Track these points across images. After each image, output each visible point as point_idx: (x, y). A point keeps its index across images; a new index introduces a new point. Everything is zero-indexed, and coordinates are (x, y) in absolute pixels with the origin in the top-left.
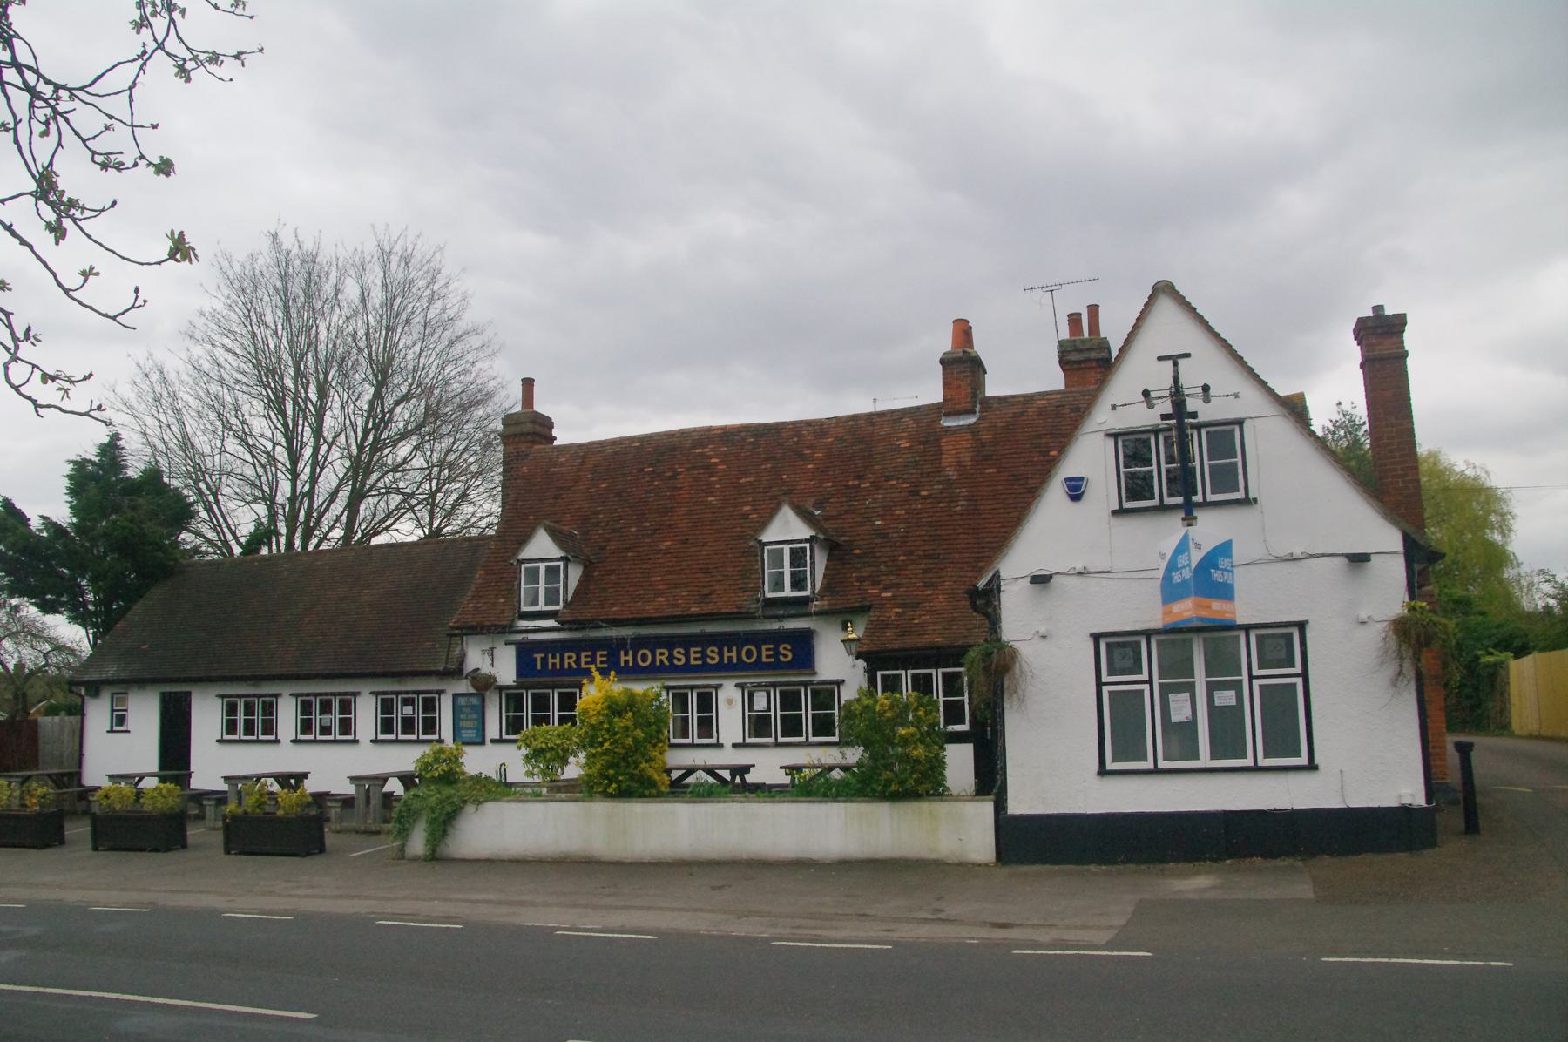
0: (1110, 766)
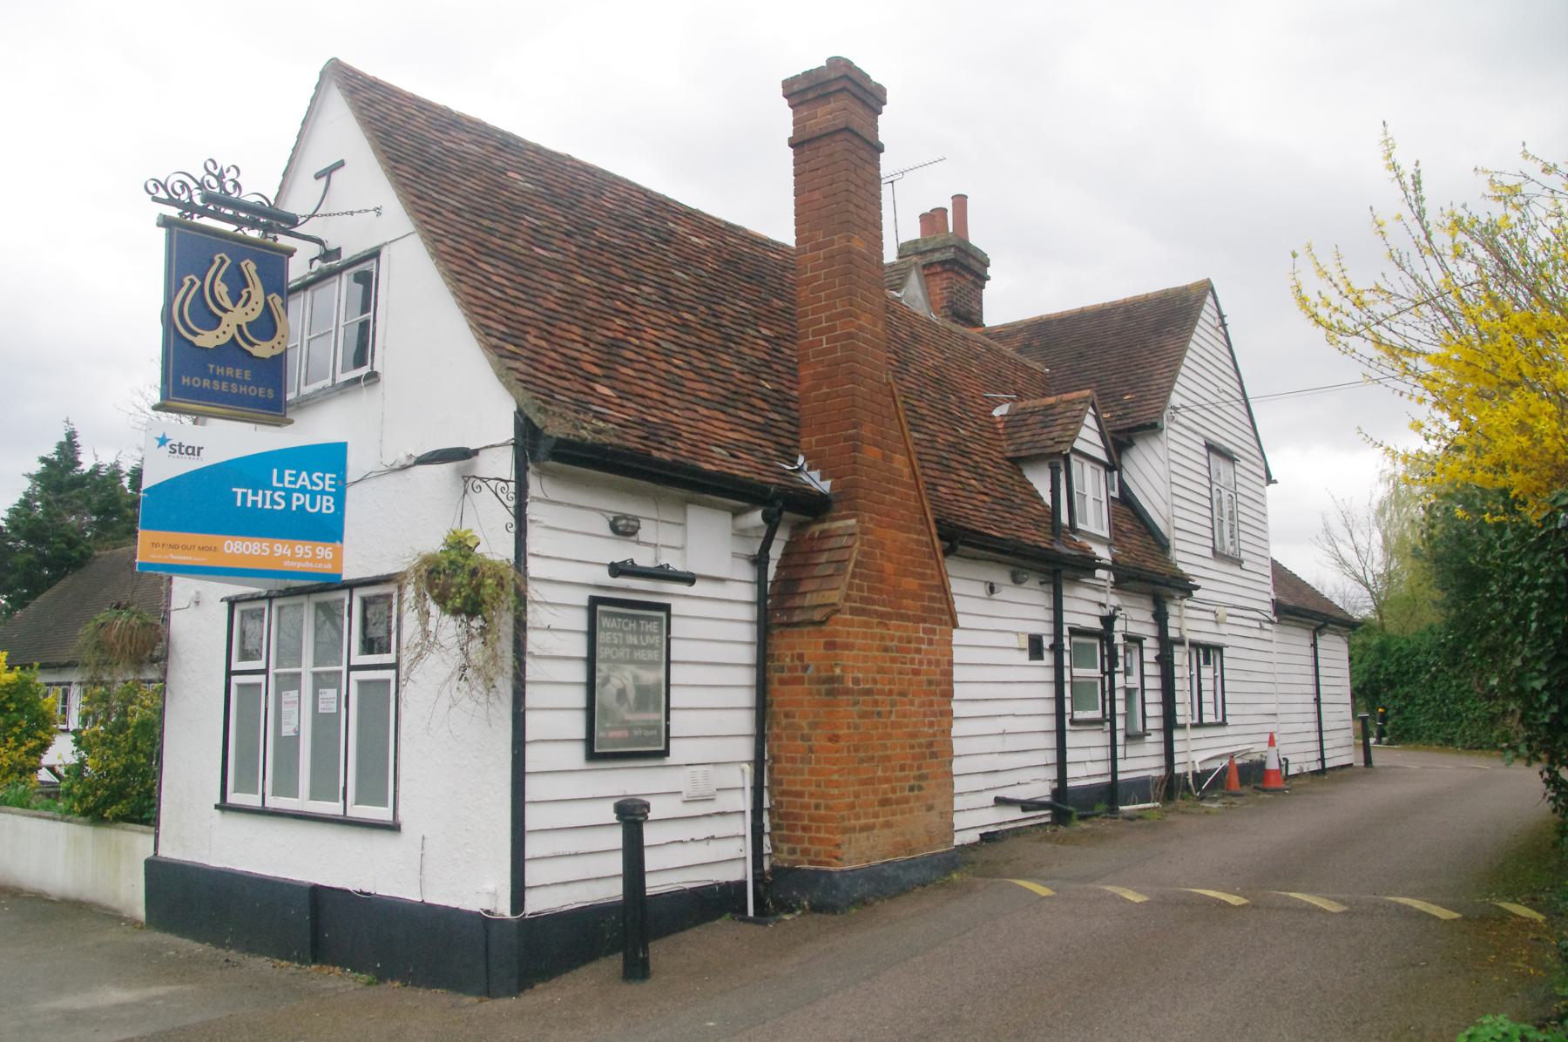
0: (233, 798)
